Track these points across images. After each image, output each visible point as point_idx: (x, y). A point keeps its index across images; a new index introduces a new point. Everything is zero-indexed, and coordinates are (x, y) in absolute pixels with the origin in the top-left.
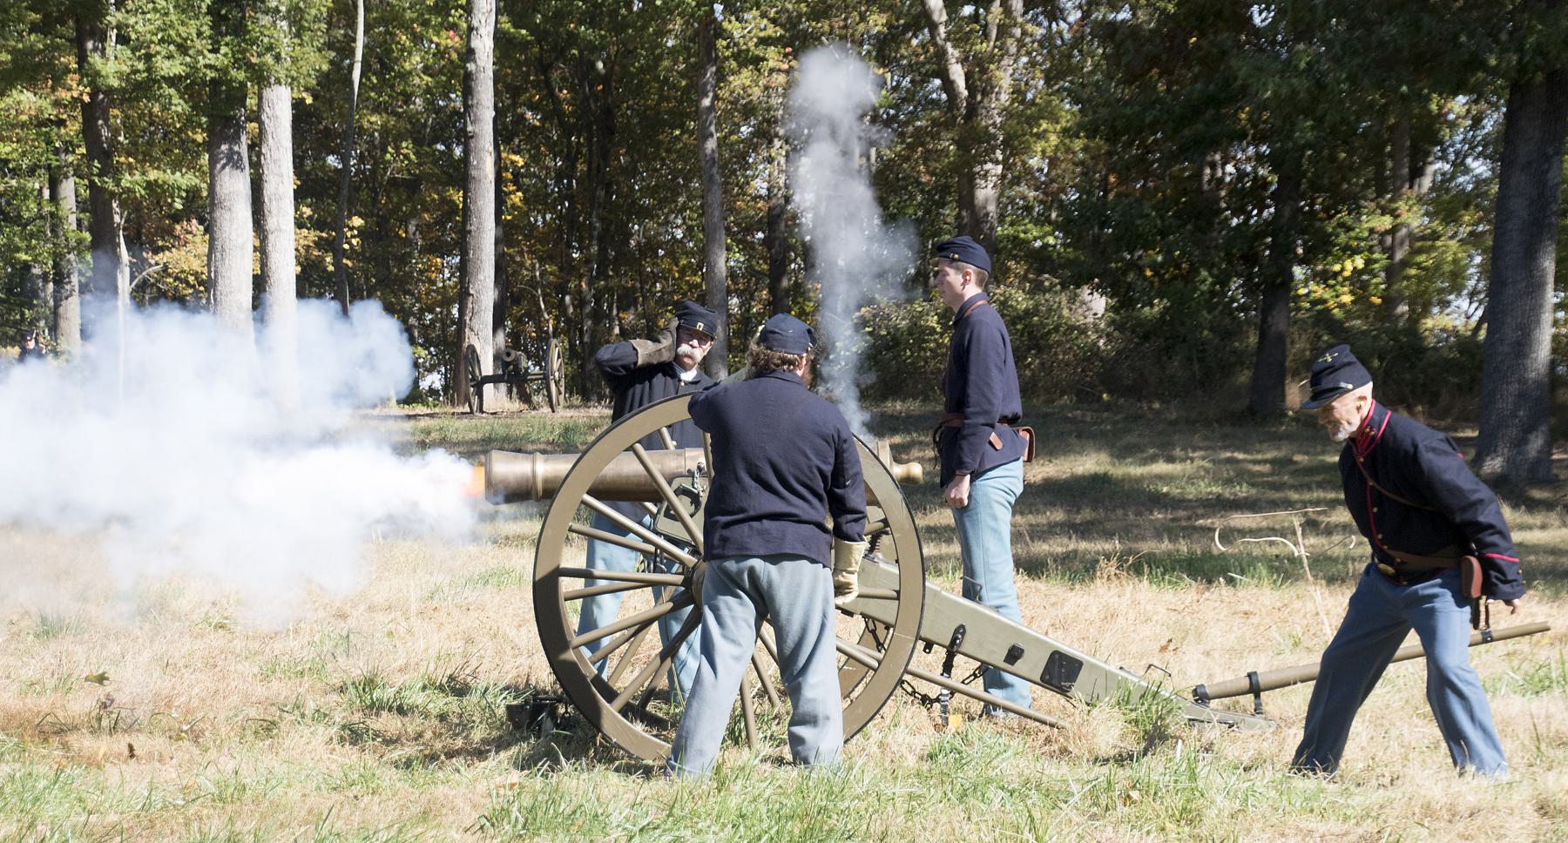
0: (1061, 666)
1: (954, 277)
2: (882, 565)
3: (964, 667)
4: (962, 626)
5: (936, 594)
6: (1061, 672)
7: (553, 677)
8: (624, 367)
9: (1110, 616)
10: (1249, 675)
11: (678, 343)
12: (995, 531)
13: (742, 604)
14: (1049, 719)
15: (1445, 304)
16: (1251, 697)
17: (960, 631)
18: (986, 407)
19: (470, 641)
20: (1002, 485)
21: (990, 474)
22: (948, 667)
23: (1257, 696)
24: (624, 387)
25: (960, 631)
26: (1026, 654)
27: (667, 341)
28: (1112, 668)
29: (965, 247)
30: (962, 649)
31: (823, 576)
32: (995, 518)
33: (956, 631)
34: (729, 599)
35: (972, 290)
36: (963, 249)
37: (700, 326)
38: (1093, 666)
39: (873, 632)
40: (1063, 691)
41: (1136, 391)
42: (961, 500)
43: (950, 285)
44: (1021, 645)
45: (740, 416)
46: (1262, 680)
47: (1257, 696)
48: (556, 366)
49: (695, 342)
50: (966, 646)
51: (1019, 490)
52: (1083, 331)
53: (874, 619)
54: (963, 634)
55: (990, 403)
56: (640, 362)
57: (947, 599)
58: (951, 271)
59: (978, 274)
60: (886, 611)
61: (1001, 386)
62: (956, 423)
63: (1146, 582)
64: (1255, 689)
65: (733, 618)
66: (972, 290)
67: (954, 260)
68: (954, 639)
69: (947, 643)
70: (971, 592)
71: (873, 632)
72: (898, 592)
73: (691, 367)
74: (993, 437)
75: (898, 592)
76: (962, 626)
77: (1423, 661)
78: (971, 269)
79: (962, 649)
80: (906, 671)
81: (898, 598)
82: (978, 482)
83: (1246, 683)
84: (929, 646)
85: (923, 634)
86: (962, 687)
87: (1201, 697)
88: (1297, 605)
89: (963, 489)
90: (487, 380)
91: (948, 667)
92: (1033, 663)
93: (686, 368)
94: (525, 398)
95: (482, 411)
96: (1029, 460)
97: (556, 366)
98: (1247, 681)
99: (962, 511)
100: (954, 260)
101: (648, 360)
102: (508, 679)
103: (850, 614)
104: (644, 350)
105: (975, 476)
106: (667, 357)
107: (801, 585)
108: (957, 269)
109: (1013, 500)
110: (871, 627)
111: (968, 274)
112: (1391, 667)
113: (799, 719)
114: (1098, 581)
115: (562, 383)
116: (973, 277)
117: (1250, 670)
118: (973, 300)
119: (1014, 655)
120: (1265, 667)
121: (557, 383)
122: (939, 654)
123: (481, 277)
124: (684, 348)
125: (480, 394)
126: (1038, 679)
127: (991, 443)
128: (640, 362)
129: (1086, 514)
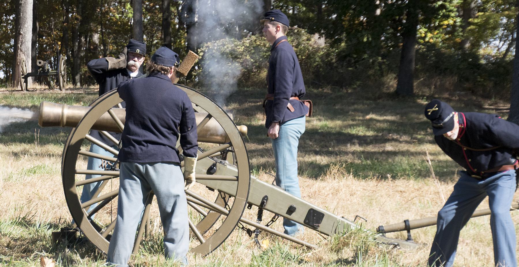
0: (314, 216)
1: (272, 29)
2: (228, 167)
3: (267, 216)
4: (266, 196)
5: (254, 180)
6: (314, 219)
7: (72, 219)
8: (102, 69)
9: (337, 191)
10: (405, 221)
11: (128, 60)
12: (290, 151)
13: (135, 180)
14: (301, 241)
15: (487, 42)
16: (405, 233)
17: (266, 198)
18: (284, 90)
19: (30, 201)
20: (295, 127)
21: (286, 124)
22: (260, 218)
23: (409, 232)
24: (102, 77)
25: (266, 198)
26: (297, 209)
27: (123, 58)
28: (339, 217)
29: (277, 14)
30: (267, 207)
31: (176, 171)
32: (289, 144)
33: (264, 199)
34: (131, 181)
35: (280, 34)
36: (277, 15)
37: (138, 51)
38: (329, 216)
39: (224, 198)
40: (315, 228)
41: (340, 83)
42: (275, 135)
43: (270, 33)
44: (295, 206)
45: (138, 93)
46: (411, 224)
47: (409, 232)
48: (62, 69)
49: (136, 59)
50: (268, 206)
51: (303, 131)
52: (328, 55)
53: (225, 193)
54: (267, 200)
55: (285, 88)
56: (109, 67)
57: (259, 183)
58: (270, 26)
59: (283, 27)
60: (230, 188)
61: (294, 80)
62: (272, 99)
63: (351, 176)
64: (408, 228)
65: (132, 190)
66: (280, 34)
67: (272, 20)
68: (263, 203)
69: (259, 204)
70: (278, 182)
71: (224, 198)
72: (237, 177)
73: (135, 70)
74: (289, 105)
75: (237, 177)
76: (266, 196)
77: (488, 217)
78: (280, 25)
79: (267, 207)
80: (227, 215)
81: (237, 180)
82: (283, 126)
83: (403, 225)
84: (250, 205)
85: (250, 200)
86: (266, 228)
87: (380, 230)
88: (426, 188)
89: (276, 129)
90: (29, 75)
91: (260, 218)
92: (299, 216)
93: (132, 71)
94: (48, 84)
95: (27, 90)
96: (310, 116)
97: (62, 69)
98: (404, 224)
99: (276, 140)
100: (272, 20)
101: (113, 67)
102: (50, 219)
103: (212, 190)
104: (112, 62)
105: (281, 124)
106: (123, 65)
107: (167, 177)
108: (273, 24)
109: (299, 136)
110: (223, 196)
111: (278, 27)
112: (472, 220)
113: (166, 239)
114: (328, 176)
115: (66, 76)
116: (281, 29)
117: (405, 219)
118: (282, 38)
119: (291, 210)
120: (413, 218)
121: (63, 76)
122: (255, 209)
123: (26, 26)
124: (131, 62)
125: (26, 82)
126: (302, 222)
127: (288, 108)
128: (109, 67)
129: (28, 134)
